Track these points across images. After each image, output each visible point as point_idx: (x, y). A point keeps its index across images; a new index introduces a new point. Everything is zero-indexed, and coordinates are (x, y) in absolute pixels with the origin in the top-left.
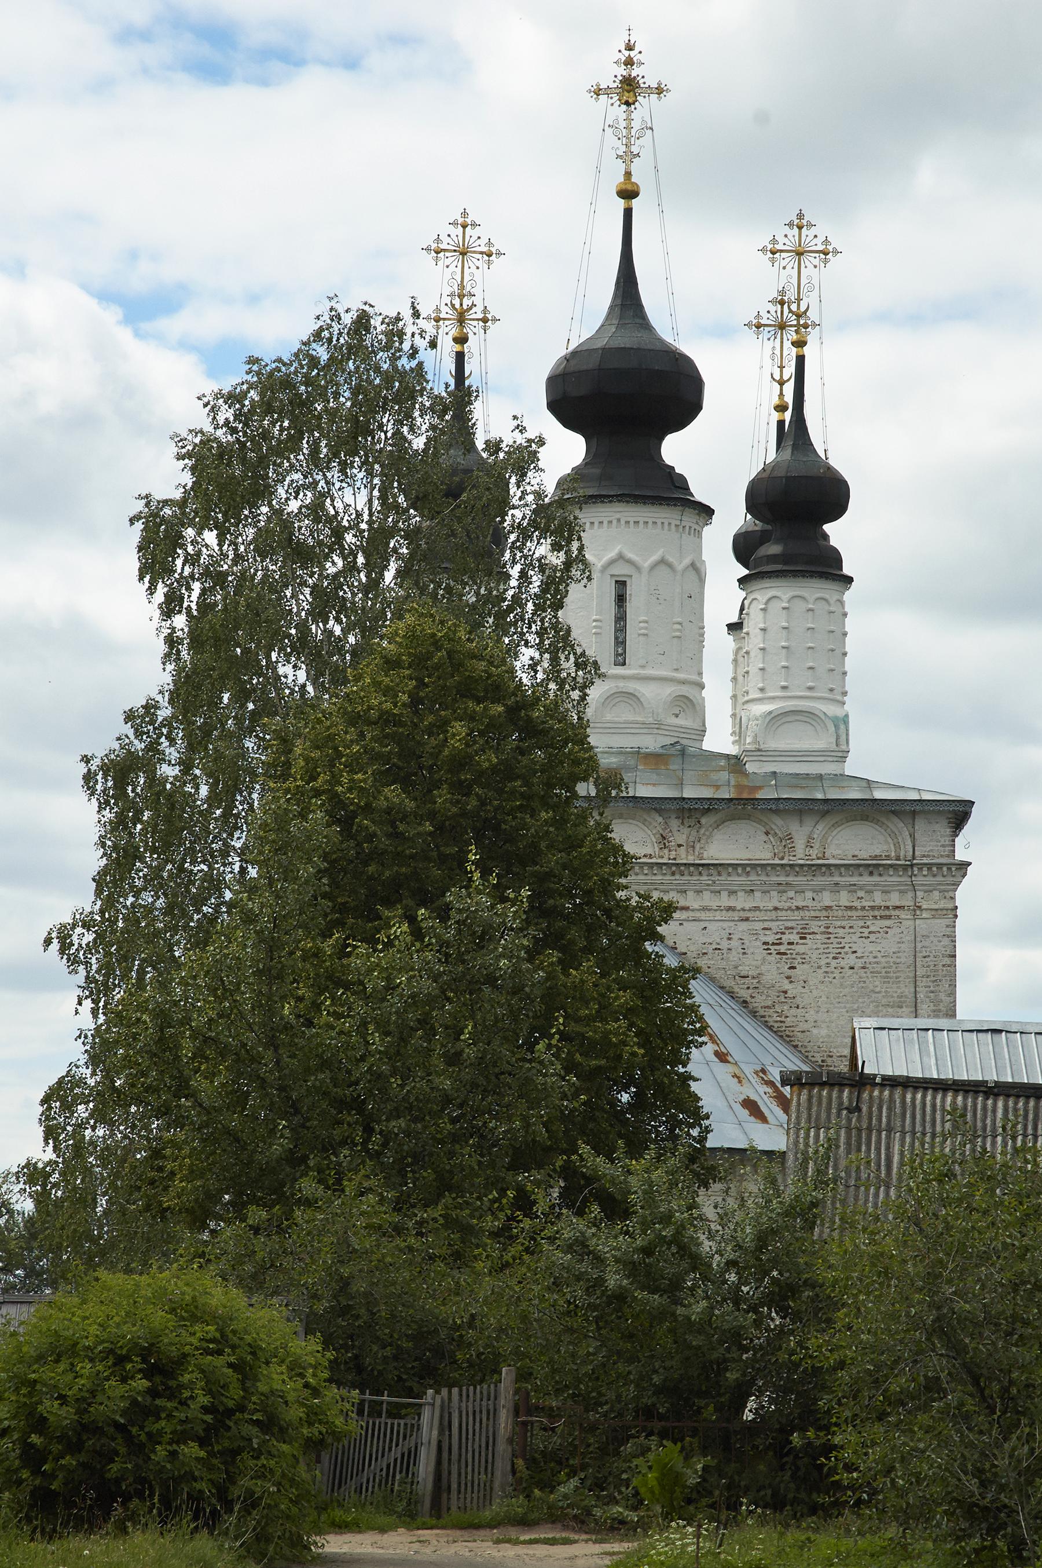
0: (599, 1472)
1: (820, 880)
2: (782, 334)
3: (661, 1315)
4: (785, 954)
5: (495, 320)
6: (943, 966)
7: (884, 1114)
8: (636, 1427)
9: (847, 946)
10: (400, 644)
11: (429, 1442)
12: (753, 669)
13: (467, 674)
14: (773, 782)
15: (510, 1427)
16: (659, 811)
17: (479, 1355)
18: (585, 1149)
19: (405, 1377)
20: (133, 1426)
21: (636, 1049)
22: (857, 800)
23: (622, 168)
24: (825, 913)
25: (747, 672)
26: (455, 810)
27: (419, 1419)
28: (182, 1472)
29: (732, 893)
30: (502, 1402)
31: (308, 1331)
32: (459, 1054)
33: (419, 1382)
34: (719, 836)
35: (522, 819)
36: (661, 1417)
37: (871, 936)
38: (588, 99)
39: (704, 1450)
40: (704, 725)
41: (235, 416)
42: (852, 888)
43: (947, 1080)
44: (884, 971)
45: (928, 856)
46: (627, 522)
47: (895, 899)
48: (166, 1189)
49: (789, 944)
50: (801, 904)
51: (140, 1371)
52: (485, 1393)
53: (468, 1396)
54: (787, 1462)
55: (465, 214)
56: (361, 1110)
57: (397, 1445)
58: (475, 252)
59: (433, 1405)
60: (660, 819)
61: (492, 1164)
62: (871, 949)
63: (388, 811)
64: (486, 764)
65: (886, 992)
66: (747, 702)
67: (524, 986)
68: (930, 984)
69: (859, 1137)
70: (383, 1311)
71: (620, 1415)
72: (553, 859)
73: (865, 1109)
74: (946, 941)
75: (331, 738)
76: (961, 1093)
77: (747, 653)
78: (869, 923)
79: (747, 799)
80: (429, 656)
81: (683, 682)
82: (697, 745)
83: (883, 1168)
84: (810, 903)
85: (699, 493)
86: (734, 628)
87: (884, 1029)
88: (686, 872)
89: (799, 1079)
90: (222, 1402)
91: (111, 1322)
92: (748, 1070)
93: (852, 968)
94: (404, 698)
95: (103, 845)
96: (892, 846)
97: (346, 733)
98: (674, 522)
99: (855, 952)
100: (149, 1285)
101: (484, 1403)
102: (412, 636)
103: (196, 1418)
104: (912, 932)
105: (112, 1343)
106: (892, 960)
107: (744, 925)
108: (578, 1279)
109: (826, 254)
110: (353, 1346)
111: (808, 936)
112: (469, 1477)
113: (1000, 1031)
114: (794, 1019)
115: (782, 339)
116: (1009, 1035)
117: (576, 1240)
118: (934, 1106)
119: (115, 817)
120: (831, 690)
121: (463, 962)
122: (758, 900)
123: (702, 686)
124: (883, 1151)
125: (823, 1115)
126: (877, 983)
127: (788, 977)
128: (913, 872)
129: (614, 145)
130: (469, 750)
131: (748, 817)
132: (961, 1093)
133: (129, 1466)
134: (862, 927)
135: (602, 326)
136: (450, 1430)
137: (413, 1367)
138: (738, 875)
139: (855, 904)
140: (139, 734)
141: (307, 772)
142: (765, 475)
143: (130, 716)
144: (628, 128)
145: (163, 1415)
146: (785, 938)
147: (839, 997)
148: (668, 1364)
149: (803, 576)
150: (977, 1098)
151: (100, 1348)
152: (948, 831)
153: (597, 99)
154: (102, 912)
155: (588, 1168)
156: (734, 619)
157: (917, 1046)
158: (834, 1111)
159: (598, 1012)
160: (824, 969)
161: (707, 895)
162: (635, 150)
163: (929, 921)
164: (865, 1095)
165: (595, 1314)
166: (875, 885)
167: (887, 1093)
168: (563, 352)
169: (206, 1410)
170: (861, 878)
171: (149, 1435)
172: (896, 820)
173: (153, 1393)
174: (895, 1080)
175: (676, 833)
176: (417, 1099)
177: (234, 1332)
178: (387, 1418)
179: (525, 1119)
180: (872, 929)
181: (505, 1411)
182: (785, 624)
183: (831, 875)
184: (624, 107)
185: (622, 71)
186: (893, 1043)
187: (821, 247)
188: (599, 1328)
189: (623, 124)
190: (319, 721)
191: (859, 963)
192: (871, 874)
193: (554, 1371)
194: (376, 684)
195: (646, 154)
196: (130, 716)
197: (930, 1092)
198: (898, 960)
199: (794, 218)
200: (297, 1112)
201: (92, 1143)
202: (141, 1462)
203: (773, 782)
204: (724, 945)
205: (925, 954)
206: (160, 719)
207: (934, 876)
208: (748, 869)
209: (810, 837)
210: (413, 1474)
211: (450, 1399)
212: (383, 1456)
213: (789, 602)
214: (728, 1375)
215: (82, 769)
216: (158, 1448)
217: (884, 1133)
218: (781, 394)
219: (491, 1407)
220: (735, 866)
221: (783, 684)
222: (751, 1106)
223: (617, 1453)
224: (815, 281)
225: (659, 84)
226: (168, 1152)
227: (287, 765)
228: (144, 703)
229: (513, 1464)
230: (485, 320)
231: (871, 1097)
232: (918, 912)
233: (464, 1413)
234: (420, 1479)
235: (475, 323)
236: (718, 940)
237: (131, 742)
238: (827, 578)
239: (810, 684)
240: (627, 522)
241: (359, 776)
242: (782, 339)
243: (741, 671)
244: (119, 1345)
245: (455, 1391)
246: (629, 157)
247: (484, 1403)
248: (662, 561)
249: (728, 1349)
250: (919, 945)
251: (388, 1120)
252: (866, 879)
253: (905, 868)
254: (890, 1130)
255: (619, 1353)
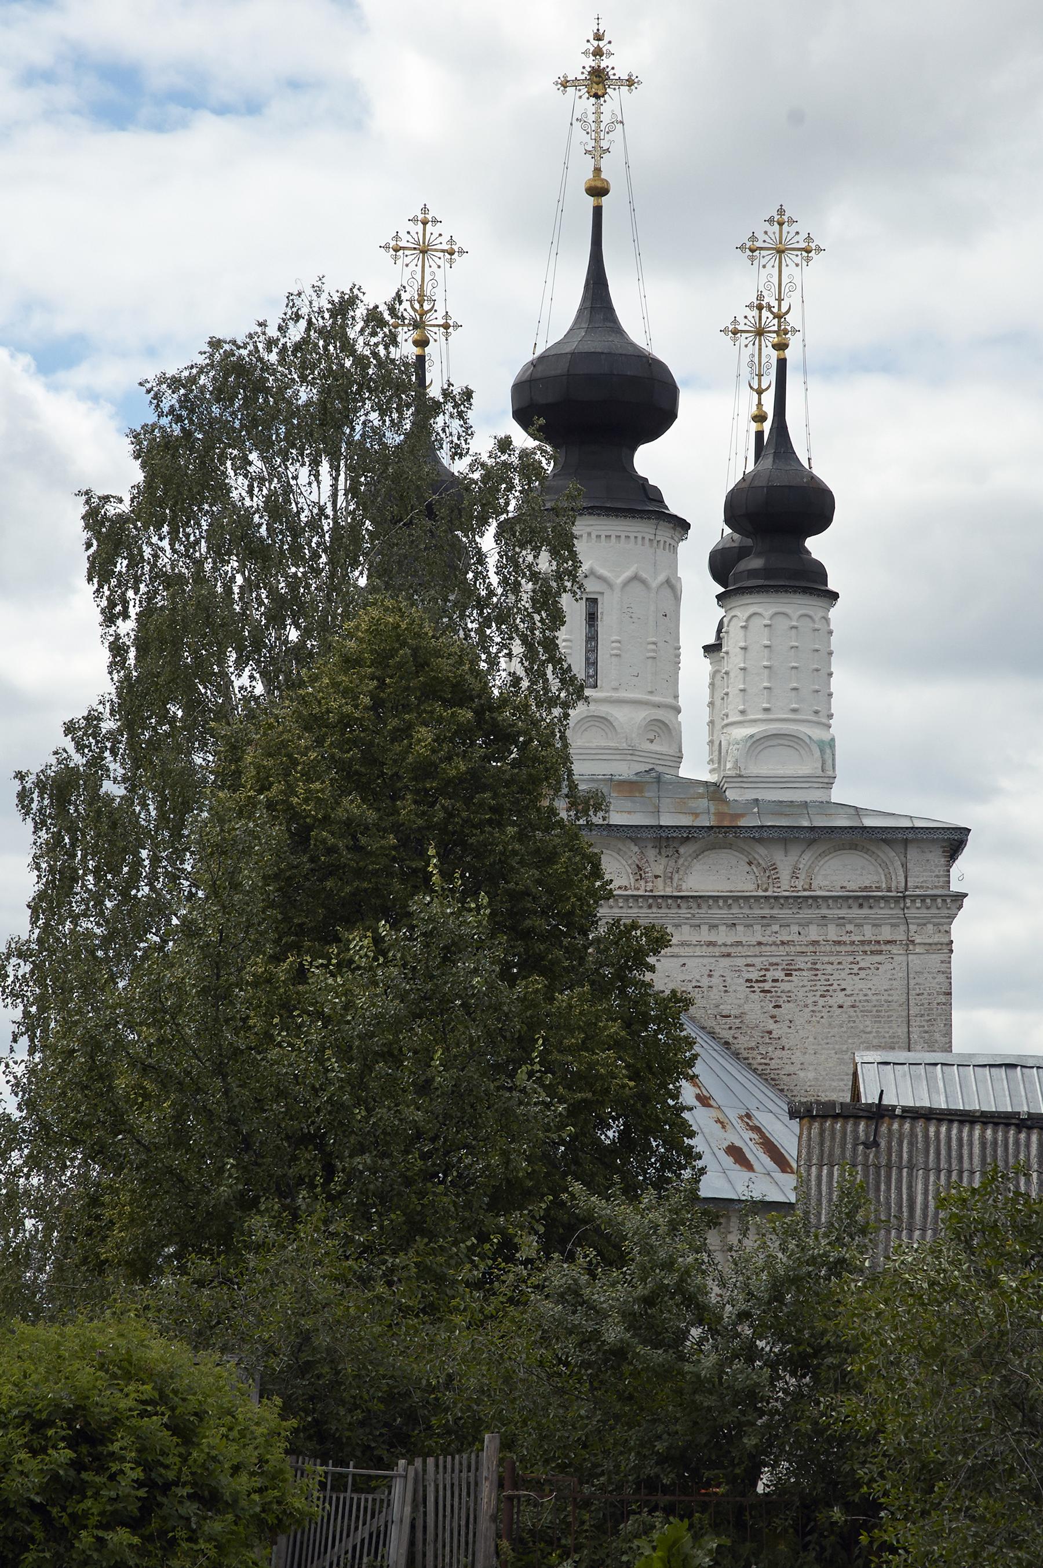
0: (594, 1553)
1: (807, 913)
2: (760, 341)
3: (665, 1373)
4: (769, 992)
5: (457, 326)
6: (938, 1004)
7: (905, 1149)
8: (637, 1501)
9: (835, 983)
10: (361, 641)
11: (401, 1521)
12: (733, 691)
13: (432, 674)
14: (756, 810)
15: (493, 1502)
16: (635, 840)
17: (457, 1420)
18: (577, 1187)
19: (373, 1445)
20: (53, 1505)
21: (626, 1081)
22: (846, 828)
23: (590, 163)
24: (811, 948)
25: (727, 694)
26: (420, 822)
27: (390, 1493)
28: (112, 1563)
29: (713, 927)
30: (485, 1474)
31: (264, 1393)
32: (429, 1081)
33: (388, 1450)
34: (698, 866)
35: (491, 834)
36: (666, 1490)
37: (861, 972)
38: (555, 92)
39: (716, 1528)
40: (680, 751)
41: (179, 401)
42: (841, 922)
43: (975, 1111)
44: (875, 1009)
45: (922, 887)
46: (598, 537)
47: (886, 934)
48: (104, 1239)
49: (774, 981)
50: (786, 938)
51: (63, 1439)
52: (465, 1463)
53: (445, 1467)
54: (810, 1542)
55: (425, 210)
56: (321, 1147)
57: (364, 1524)
58: (436, 250)
59: (406, 1477)
60: (636, 849)
61: (468, 1206)
62: (861, 987)
63: (348, 823)
64: (454, 772)
65: (877, 1032)
66: (727, 725)
67: (501, 1004)
68: (924, 1023)
69: (878, 1174)
70: (348, 1368)
71: (619, 1488)
72: (528, 876)
73: (883, 1144)
74: (941, 978)
75: (284, 744)
76: (990, 1126)
77: (727, 673)
78: (858, 959)
79: (728, 827)
80: (393, 653)
81: (658, 706)
82: (672, 771)
83: (905, 1209)
84: (795, 938)
85: (674, 505)
86: (710, 650)
87: (889, 1063)
88: (664, 905)
89: (810, 1111)
90: (161, 1475)
91: (27, 1381)
92: (732, 1115)
93: (841, 1007)
94: (367, 700)
95: (38, 868)
96: (883, 877)
97: (300, 738)
98: (648, 537)
99: (844, 989)
100: (77, 1336)
101: (464, 1475)
102: (375, 631)
103: (129, 1495)
104: (905, 968)
105: (29, 1406)
106: (883, 998)
107: (725, 962)
108: (570, 1333)
109: (808, 252)
110: (314, 1410)
111: (794, 973)
112: (447, 1560)
113: (1014, 1066)
114: (779, 1061)
115: (760, 345)
116: (1025, 1070)
117: (569, 1288)
118: (960, 1140)
119: (52, 838)
120: (816, 712)
121: (432, 977)
122: (741, 934)
123: (678, 711)
124: (904, 1191)
125: (837, 1151)
126: (868, 1023)
127: (772, 1017)
128: (905, 904)
129: (582, 139)
130: (434, 758)
131: (730, 846)
132: (990, 1126)
133: (48, 1555)
134: (852, 963)
135: (571, 330)
136: (425, 1507)
137: (381, 1435)
138: (720, 908)
139: (843, 939)
140: (80, 747)
141: (257, 782)
142: (744, 485)
143: (70, 728)
144: (597, 121)
145: (89, 1494)
146: (769, 975)
147: (827, 1038)
148: (673, 1428)
149: (786, 591)
150: (1007, 1132)
151: (15, 1412)
152: (943, 861)
153: (564, 92)
154: (40, 941)
155: (581, 1208)
156: (711, 640)
157: (925, 1083)
158: (849, 1146)
159: (583, 1042)
160: (811, 1008)
161: (686, 929)
162: (605, 145)
163: (922, 957)
164: (884, 1129)
165: (589, 1372)
166: (865, 918)
167: (907, 1126)
168: (530, 357)
169: (139, 1484)
170: (849, 911)
171: (73, 1517)
172: (887, 849)
173: (77, 1465)
174: (917, 1112)
175: (652, 864)
176: (384, 1133)
177: (175, 1392)
178: (353, 1491)
179: (505, 1154)
180: (862, 965)
181: (487, 1484)
182: (768, 643)
183: (818, 907)
184: (593, 100)
185: (590, 62)
186: (899, 1078)
187: (803, 245)
188: (593, 1389)
189: (592, 118)
190: (271, 726)
191: (849, 1001)
192: (861, 906)
193: (542, 1438)
194: (335, 684)
195: (617, 149)
196: (70, 728)
197: (955, 1125)
198: (890, 999)
199: (775, 214)
200: (248, 1147)
201: (27, 1193)
202: (62, 1550)
203: (756, 810)
204: (705, 982)
205: (918, 991)
206: (104, 731)
207: (928, 908)
208: (730, 901)
209: (795, 868)
210: (383, 1557)
211: (424, 1471)
212: (348, 1536)
213: (771, 619)
214: (745, 1441)
215: (16, 786)
216: (83, 1533)
217: (905, 1170)
218: (760, 404)
219: (472, 1480)
220: (715, 898)
221: (765, 705)
222: (735, 1153)
223: (616, 1532)
224: (797, 281)
225: (630, 75)
226: (107, 1198)
227: (238, 773)
228: (86, 714)
229: (497, 1546)
230: (446, 326)
231: (890, 1130)
232: (911, 947)
233: (441, 1487)
234: (391, 1562)
235: (435, 329)
236: (698, 978)
237: (69, 757)
238: (811, 594)
239: (794, 706)
240: (598, 537)
241: (317, 785)
242: (760, 345)
243: (719, 694)
244: (38, 1408)
245: (431, 1461)
246: (598, 152)
247: (464, 1475)
248: (636, 578)
249: (743, 1413)
250: (912, 982)
251: (351, 1156)
252: (856, 912)
253: (896, 900)
254: (911, 1167)
255: (617, 1417)
